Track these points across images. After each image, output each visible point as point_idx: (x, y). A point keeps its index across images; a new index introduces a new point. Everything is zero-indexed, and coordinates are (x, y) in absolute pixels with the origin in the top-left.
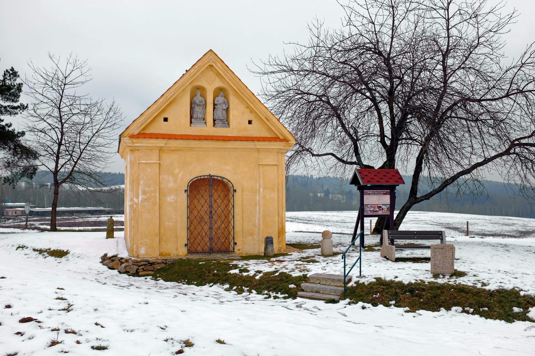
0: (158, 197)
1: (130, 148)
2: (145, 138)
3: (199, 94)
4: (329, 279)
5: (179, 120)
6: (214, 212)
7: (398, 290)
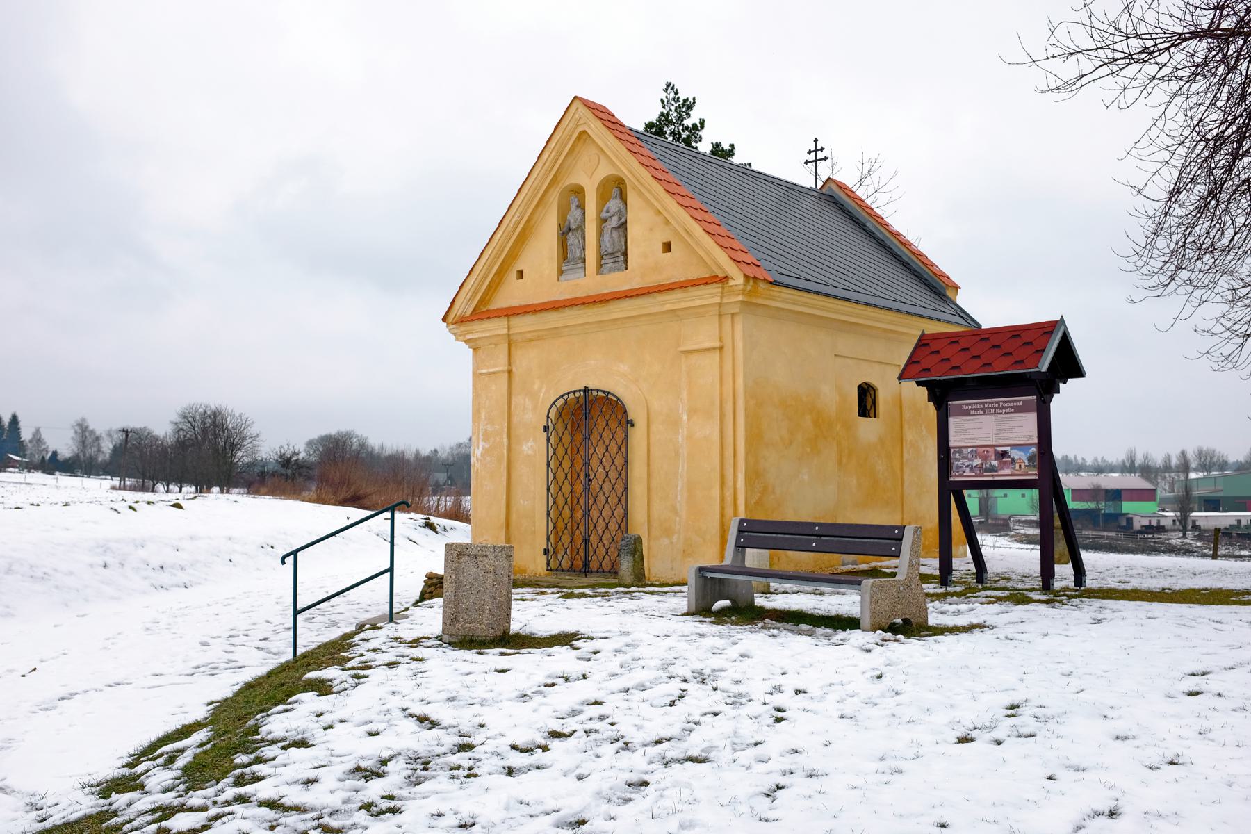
5: (540, 271)
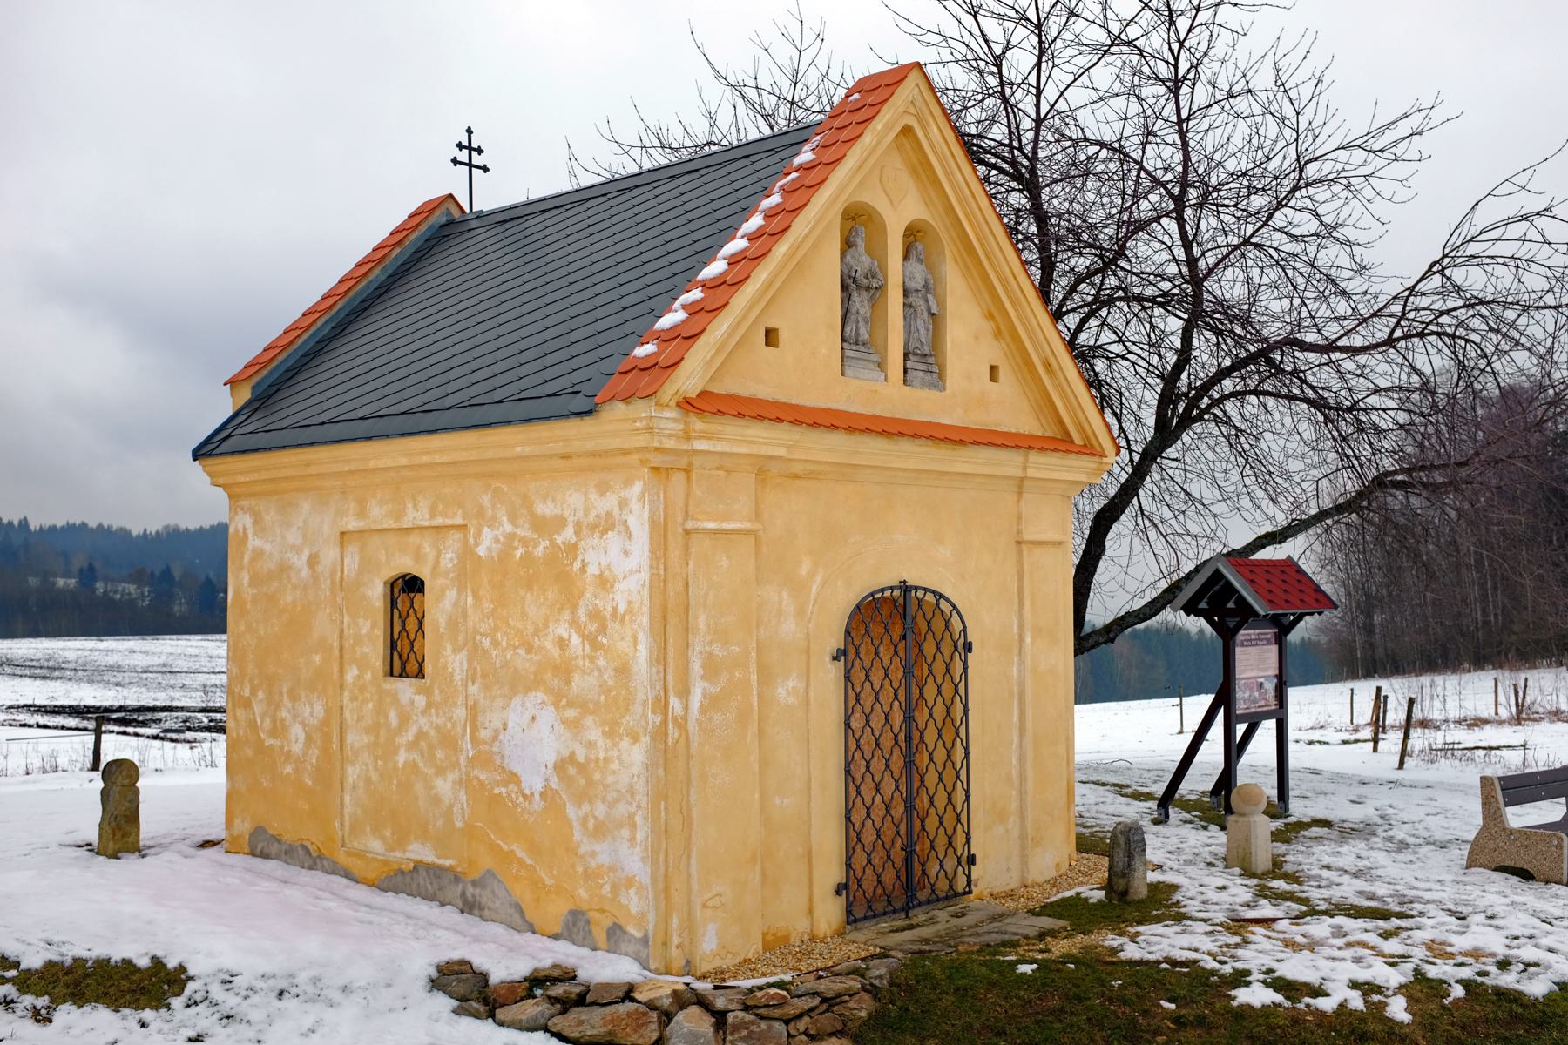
1: (657, 460)
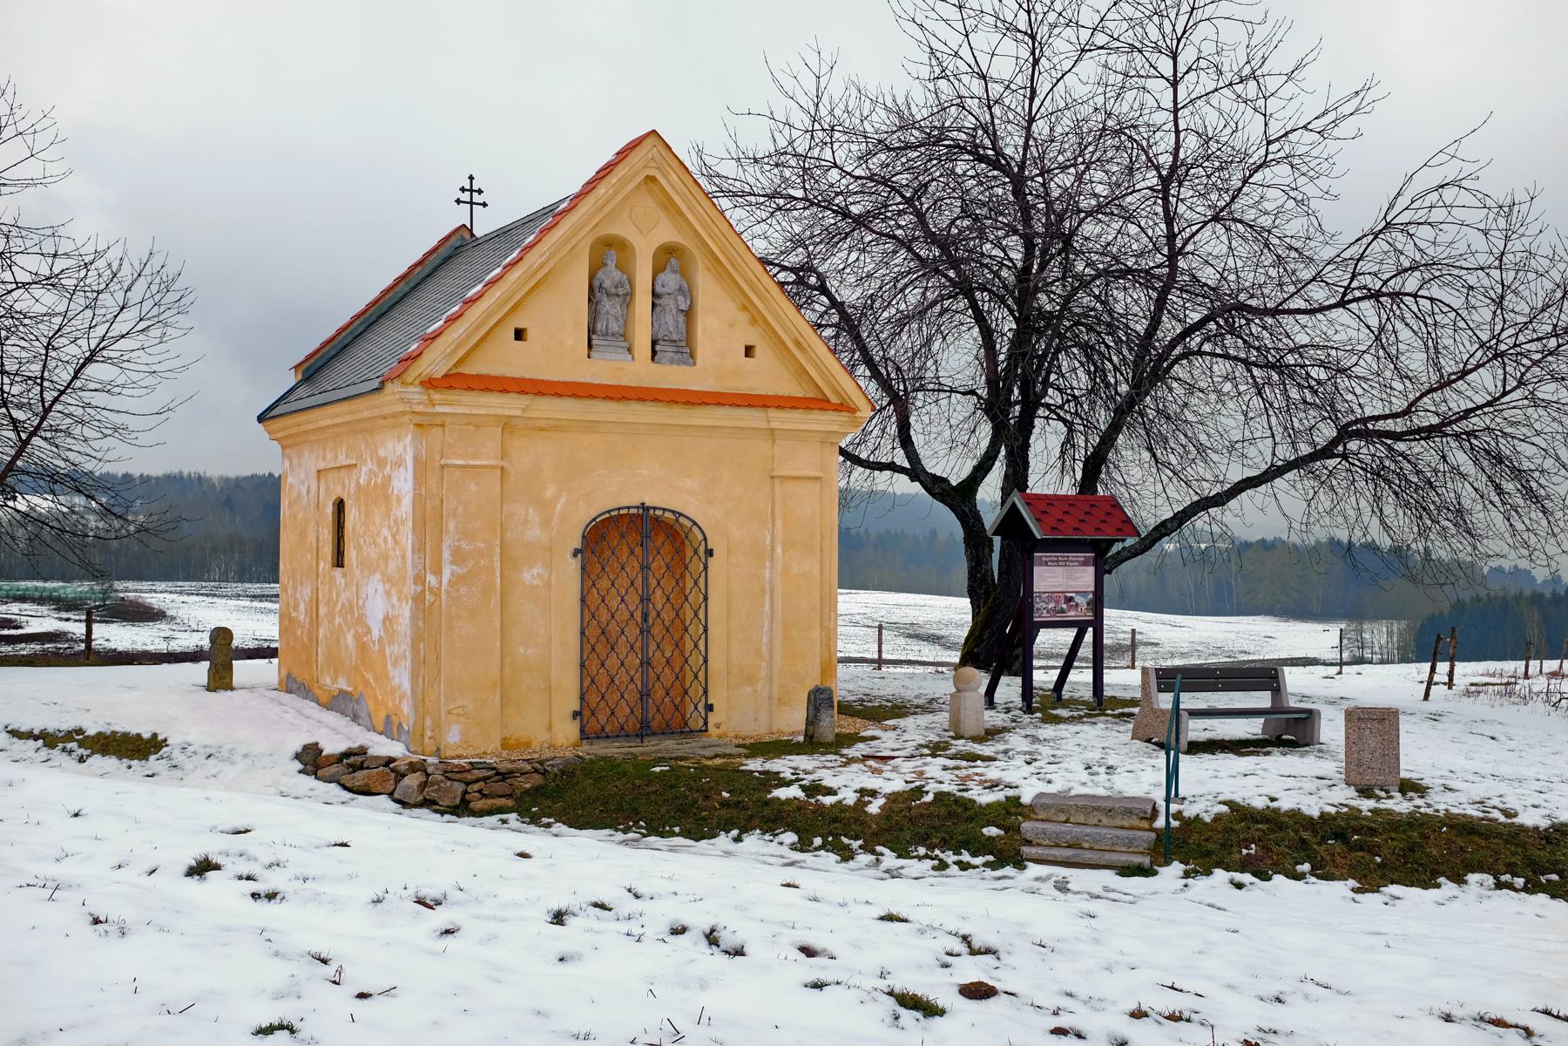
0: (498, 570)
1: (418, 419)
2: (470, 389)
3: (612, 259)
4: (1097, 809)
6: (653, 614)
7: (1306, 835)
